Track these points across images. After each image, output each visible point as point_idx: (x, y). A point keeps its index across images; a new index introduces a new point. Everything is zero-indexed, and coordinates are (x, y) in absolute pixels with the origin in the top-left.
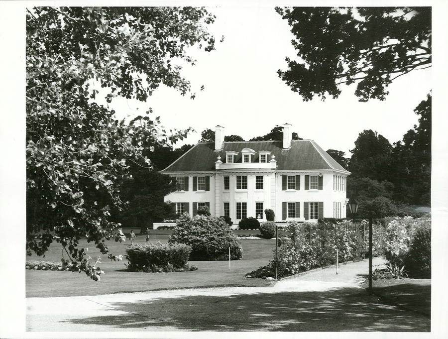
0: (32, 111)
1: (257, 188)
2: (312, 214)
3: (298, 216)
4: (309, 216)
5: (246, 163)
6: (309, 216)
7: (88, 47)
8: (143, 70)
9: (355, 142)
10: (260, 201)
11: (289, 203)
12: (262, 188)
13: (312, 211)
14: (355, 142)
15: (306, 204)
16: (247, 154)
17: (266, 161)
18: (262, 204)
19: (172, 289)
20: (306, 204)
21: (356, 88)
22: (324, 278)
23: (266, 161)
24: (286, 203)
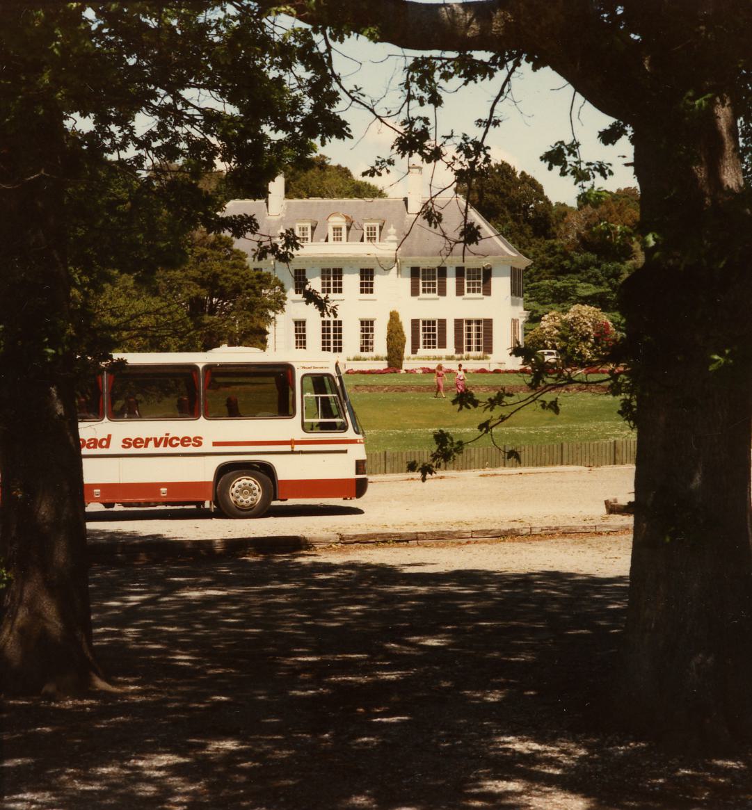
0: (467, 730)
1: (362, 291)
2: (469, 342)
3: (443, 345)
4: (465, 345)
5: (336, 242)
6: (465, 345)
7: (64, 121)
8: (159, 167)
9: (613, 144)
10: (367, 316)
11: (424, 323)
12: (372, 292)
13: (469, 336)
14: (613, 144)
15: (458, 323)
16: (337, 225)
17: (378, 239)
18: (372, 323)
19: (376, 544)
20: (458, 323)
21: (401, 319)
22: (322, 502)
23: (378, 239)
24: (418, 320)
